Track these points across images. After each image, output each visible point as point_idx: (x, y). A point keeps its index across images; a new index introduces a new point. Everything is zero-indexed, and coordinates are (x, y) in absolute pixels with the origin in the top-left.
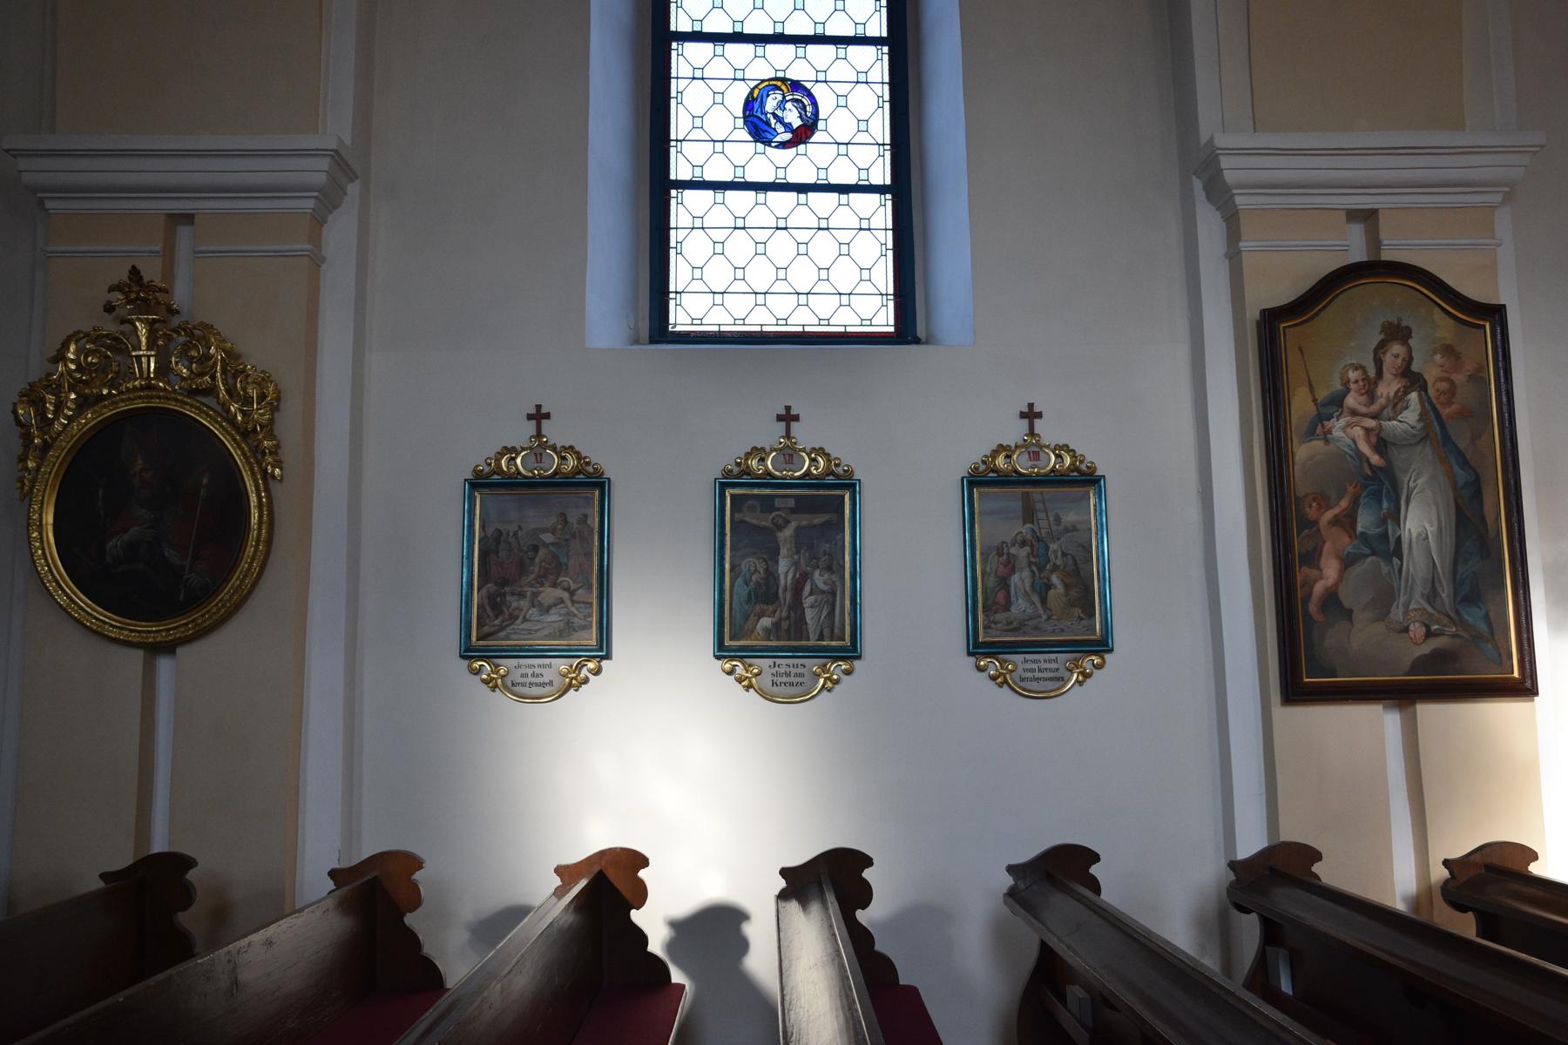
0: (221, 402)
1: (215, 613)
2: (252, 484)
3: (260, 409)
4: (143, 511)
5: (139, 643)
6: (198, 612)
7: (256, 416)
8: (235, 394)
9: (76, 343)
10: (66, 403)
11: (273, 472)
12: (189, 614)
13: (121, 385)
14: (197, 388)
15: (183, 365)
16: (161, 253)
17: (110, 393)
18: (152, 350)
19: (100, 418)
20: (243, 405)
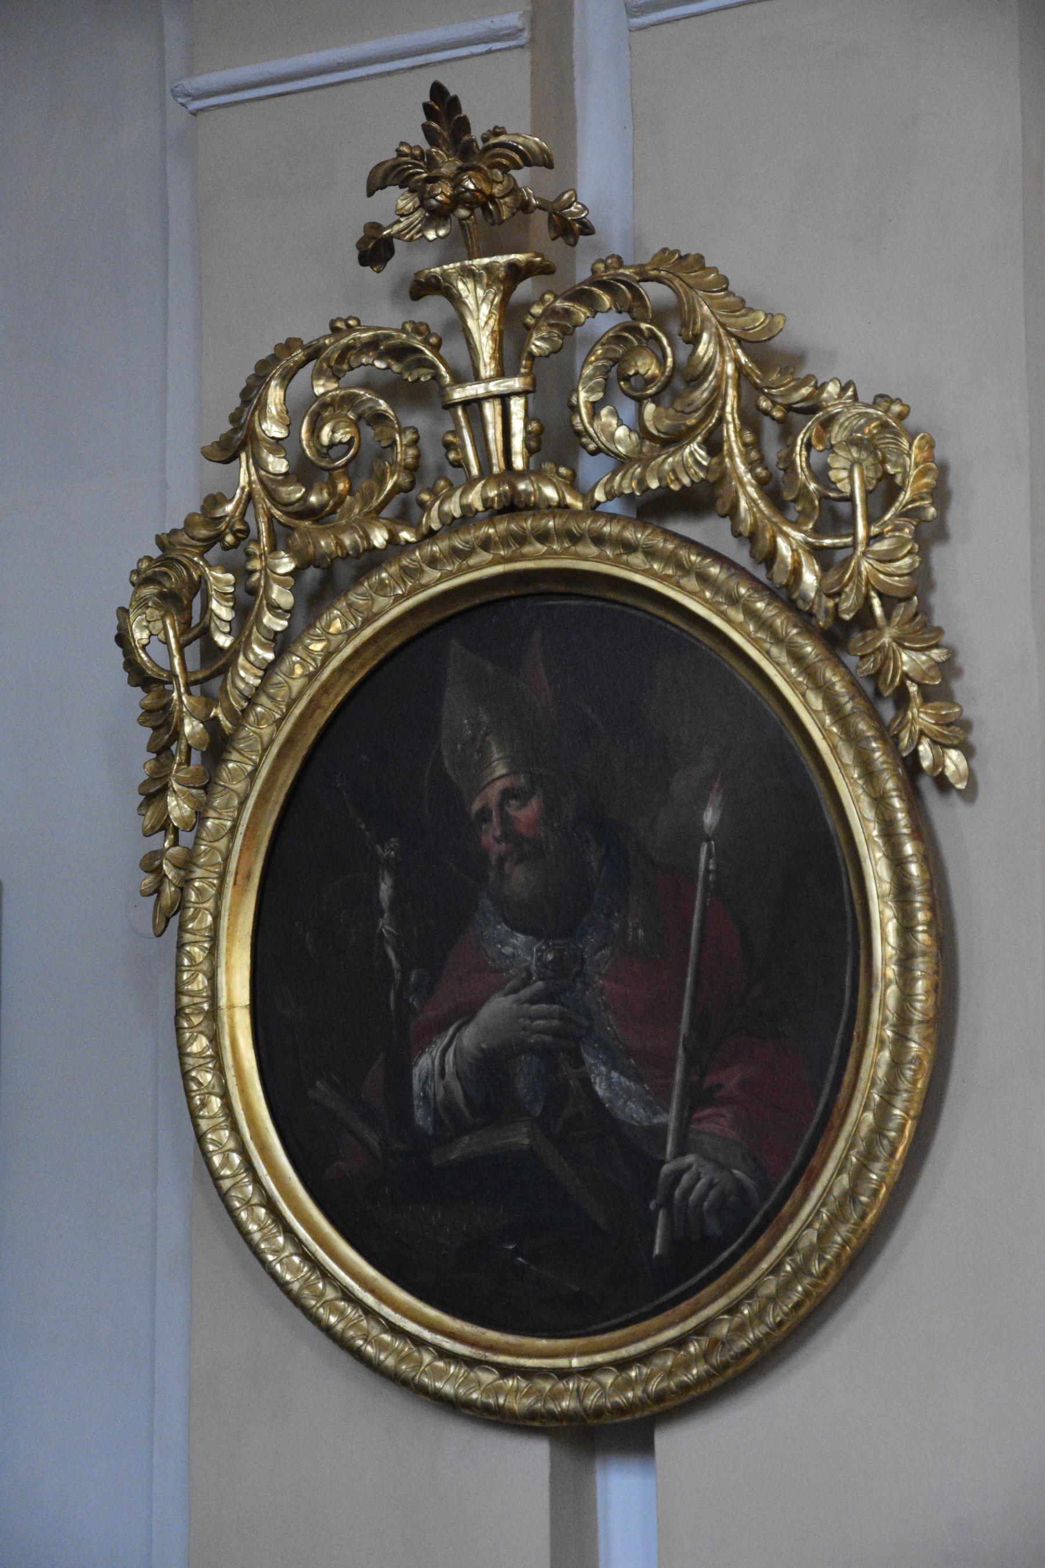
0: (746, 528)
1: (773, 1299)
2: (870, 814)
3: (880, 537)
4: (520, 939)
5: (532, 1415)
6: (713, 1300)
7: (865, 565)
8: (788, 496)
9: (287, 378)
10: (267, 588)
11: (938, 762)
12: (684, 1306)
13: (424, 507)
14: (664, 488)
15: (615, 413)
16: (526, 35)
17: (393, 540)
18: (516, 373)
19: (368, 632)
20: (818, 531)
